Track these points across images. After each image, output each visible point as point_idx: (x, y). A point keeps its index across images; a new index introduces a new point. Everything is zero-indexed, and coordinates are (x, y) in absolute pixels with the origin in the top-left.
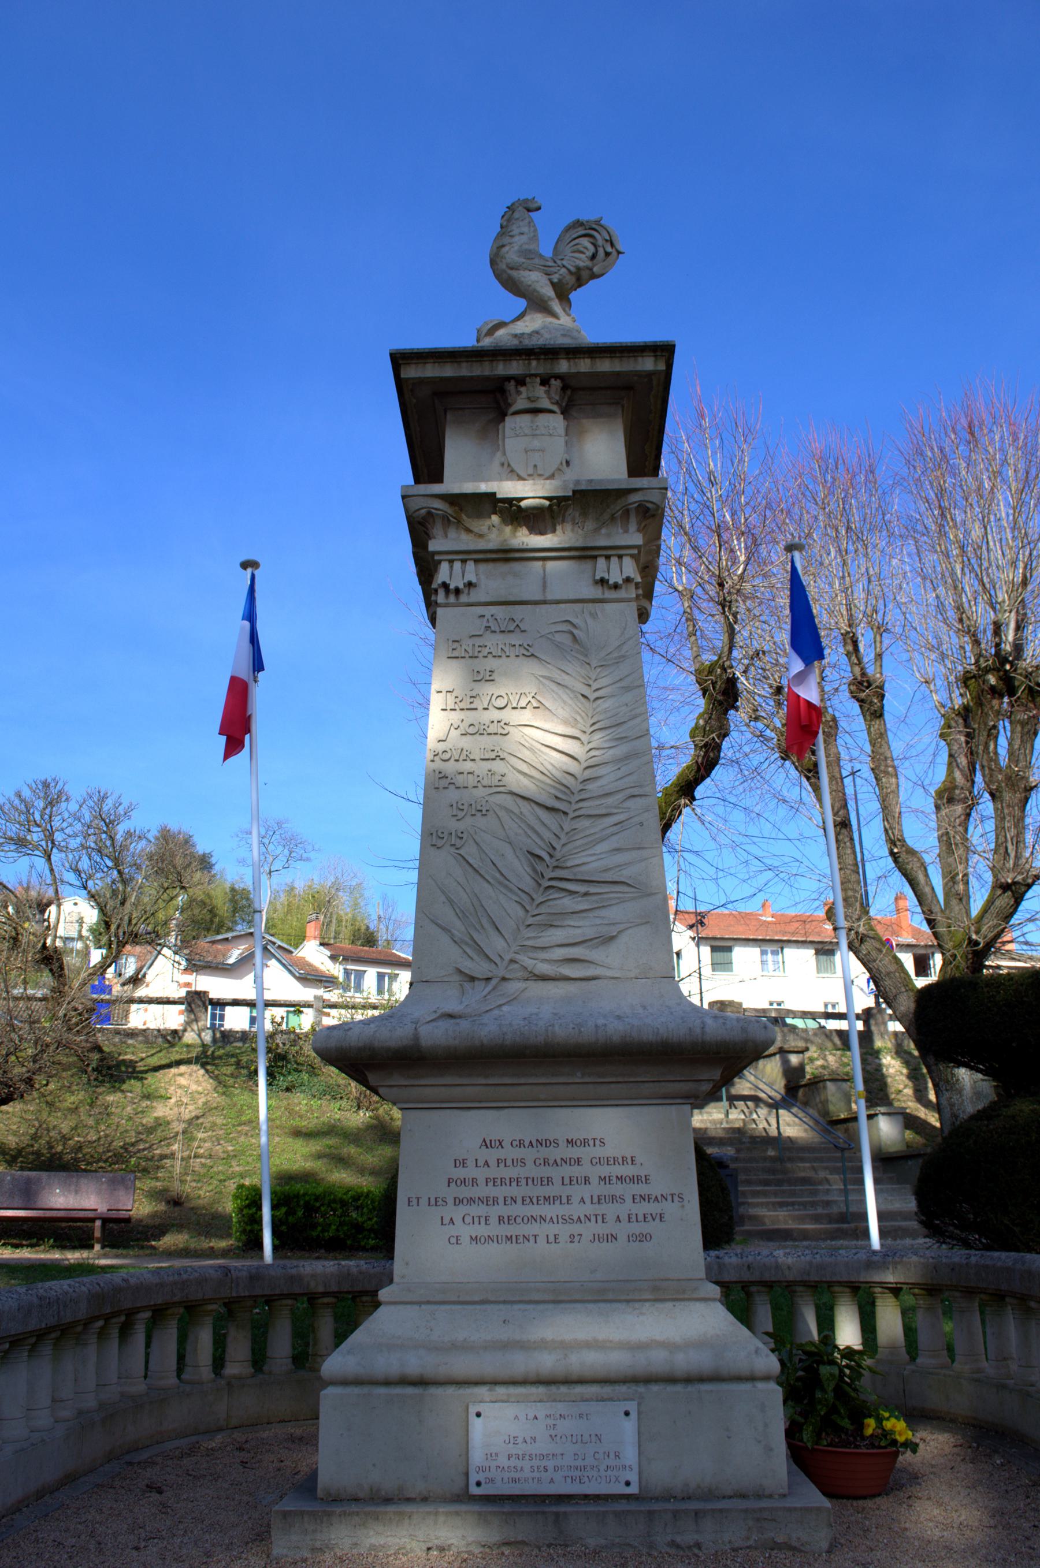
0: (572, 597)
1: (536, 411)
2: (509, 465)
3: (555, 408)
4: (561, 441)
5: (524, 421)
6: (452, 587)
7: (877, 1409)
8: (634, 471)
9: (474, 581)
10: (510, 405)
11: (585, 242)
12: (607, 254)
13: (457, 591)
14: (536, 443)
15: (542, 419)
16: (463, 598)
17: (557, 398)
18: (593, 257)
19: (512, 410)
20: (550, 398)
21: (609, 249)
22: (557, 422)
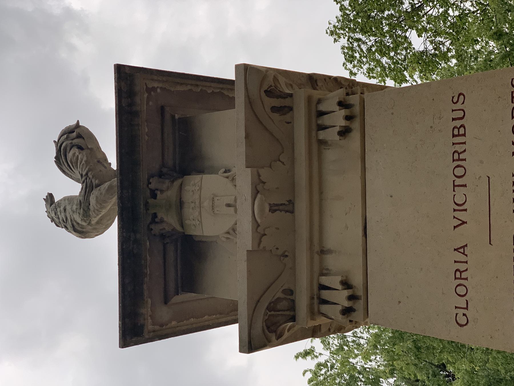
0: (491, 239)
1: (181, 204)
2: (228, 233)
3: (177, 183)
4: (206, 177)
5: (190, 213)
6: (347, 304)
7: (440, 55)
8: (230, 103)
9: (339, 278)
10: (174, 229)
11: (70, 155)
12: (79, 136)
13: (352, 298)
14: (206, 204)
15: (189, 196)
16: (360, 292)
17: (167, 181)
18: (80, 148)
19: (179, 228)
20: (168, 189)
21: (74, 134)
22: (193, 181)
